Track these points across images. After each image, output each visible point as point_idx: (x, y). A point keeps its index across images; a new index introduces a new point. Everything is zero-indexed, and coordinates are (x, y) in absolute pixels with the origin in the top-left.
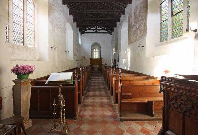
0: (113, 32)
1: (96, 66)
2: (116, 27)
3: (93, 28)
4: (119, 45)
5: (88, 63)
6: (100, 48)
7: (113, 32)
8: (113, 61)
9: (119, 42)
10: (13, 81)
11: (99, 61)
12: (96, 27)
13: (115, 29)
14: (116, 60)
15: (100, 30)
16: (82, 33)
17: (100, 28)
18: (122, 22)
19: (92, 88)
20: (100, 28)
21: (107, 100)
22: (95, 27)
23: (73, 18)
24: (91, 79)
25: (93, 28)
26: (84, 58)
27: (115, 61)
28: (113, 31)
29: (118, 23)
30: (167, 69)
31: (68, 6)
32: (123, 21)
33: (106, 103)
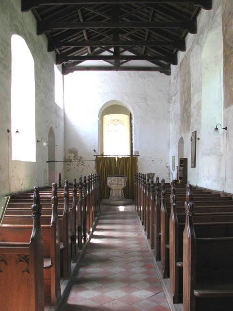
0: (173, 67)
1: (116, 184)
2: (183, 48)
3: (106, 53)
4: (194, 111)
5: (91, 170)
6: (131, 119)
7: (173, 67)
8: (177, 164)
9: (194, 103)
10: (182, 137)
11: (128, 165)
12: (116, 49)
13: (181, 55)
14: (186, 159)
15: (129, 58)
16: (65, 71)
17: (128, 53)
18: (202, 33)
19: (94, 270)
20: (128, 53)
21: (149, 294)
22: (112, 50)
23: (35, 21)
24: (95, 233)
25: (106, 53)
26: (73, 155)
27: (183, 162)
28: (175, 63)
29: (190, 37)
30: (18, 133)
31: (176, 214)
32: (206, 30)
33: (145, 301)
